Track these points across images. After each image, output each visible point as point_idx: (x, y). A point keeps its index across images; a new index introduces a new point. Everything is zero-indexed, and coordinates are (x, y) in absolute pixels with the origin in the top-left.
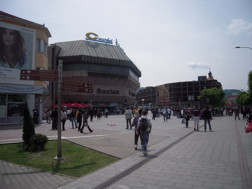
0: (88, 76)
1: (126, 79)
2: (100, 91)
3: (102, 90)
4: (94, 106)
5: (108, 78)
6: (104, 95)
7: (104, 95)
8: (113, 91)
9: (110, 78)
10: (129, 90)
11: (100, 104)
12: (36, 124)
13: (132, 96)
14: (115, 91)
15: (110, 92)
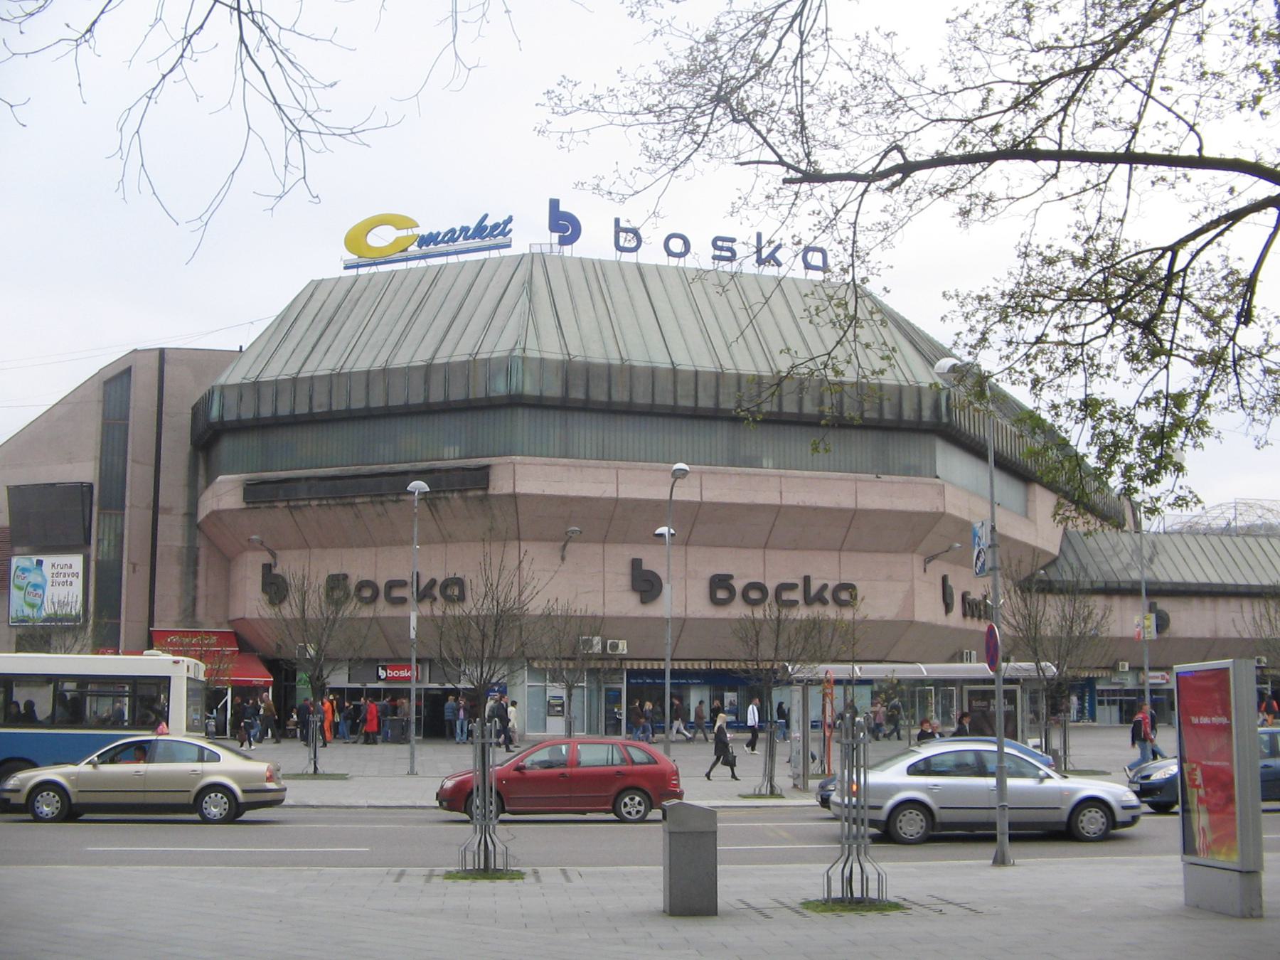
0: (247, 503)
1: (480, 493)
2: (731, 590)
3: (739, 585)
4: (358, 686)
5: (358, 500)
6: (367, 612)
7: (367, 612)
8: (815, 587)
9: (369, 499)
10: (945, 579)
11: (382, 673)
12: (203, 734)
13: (965, 615)
14: (440, 580)
15: (797, 595)
